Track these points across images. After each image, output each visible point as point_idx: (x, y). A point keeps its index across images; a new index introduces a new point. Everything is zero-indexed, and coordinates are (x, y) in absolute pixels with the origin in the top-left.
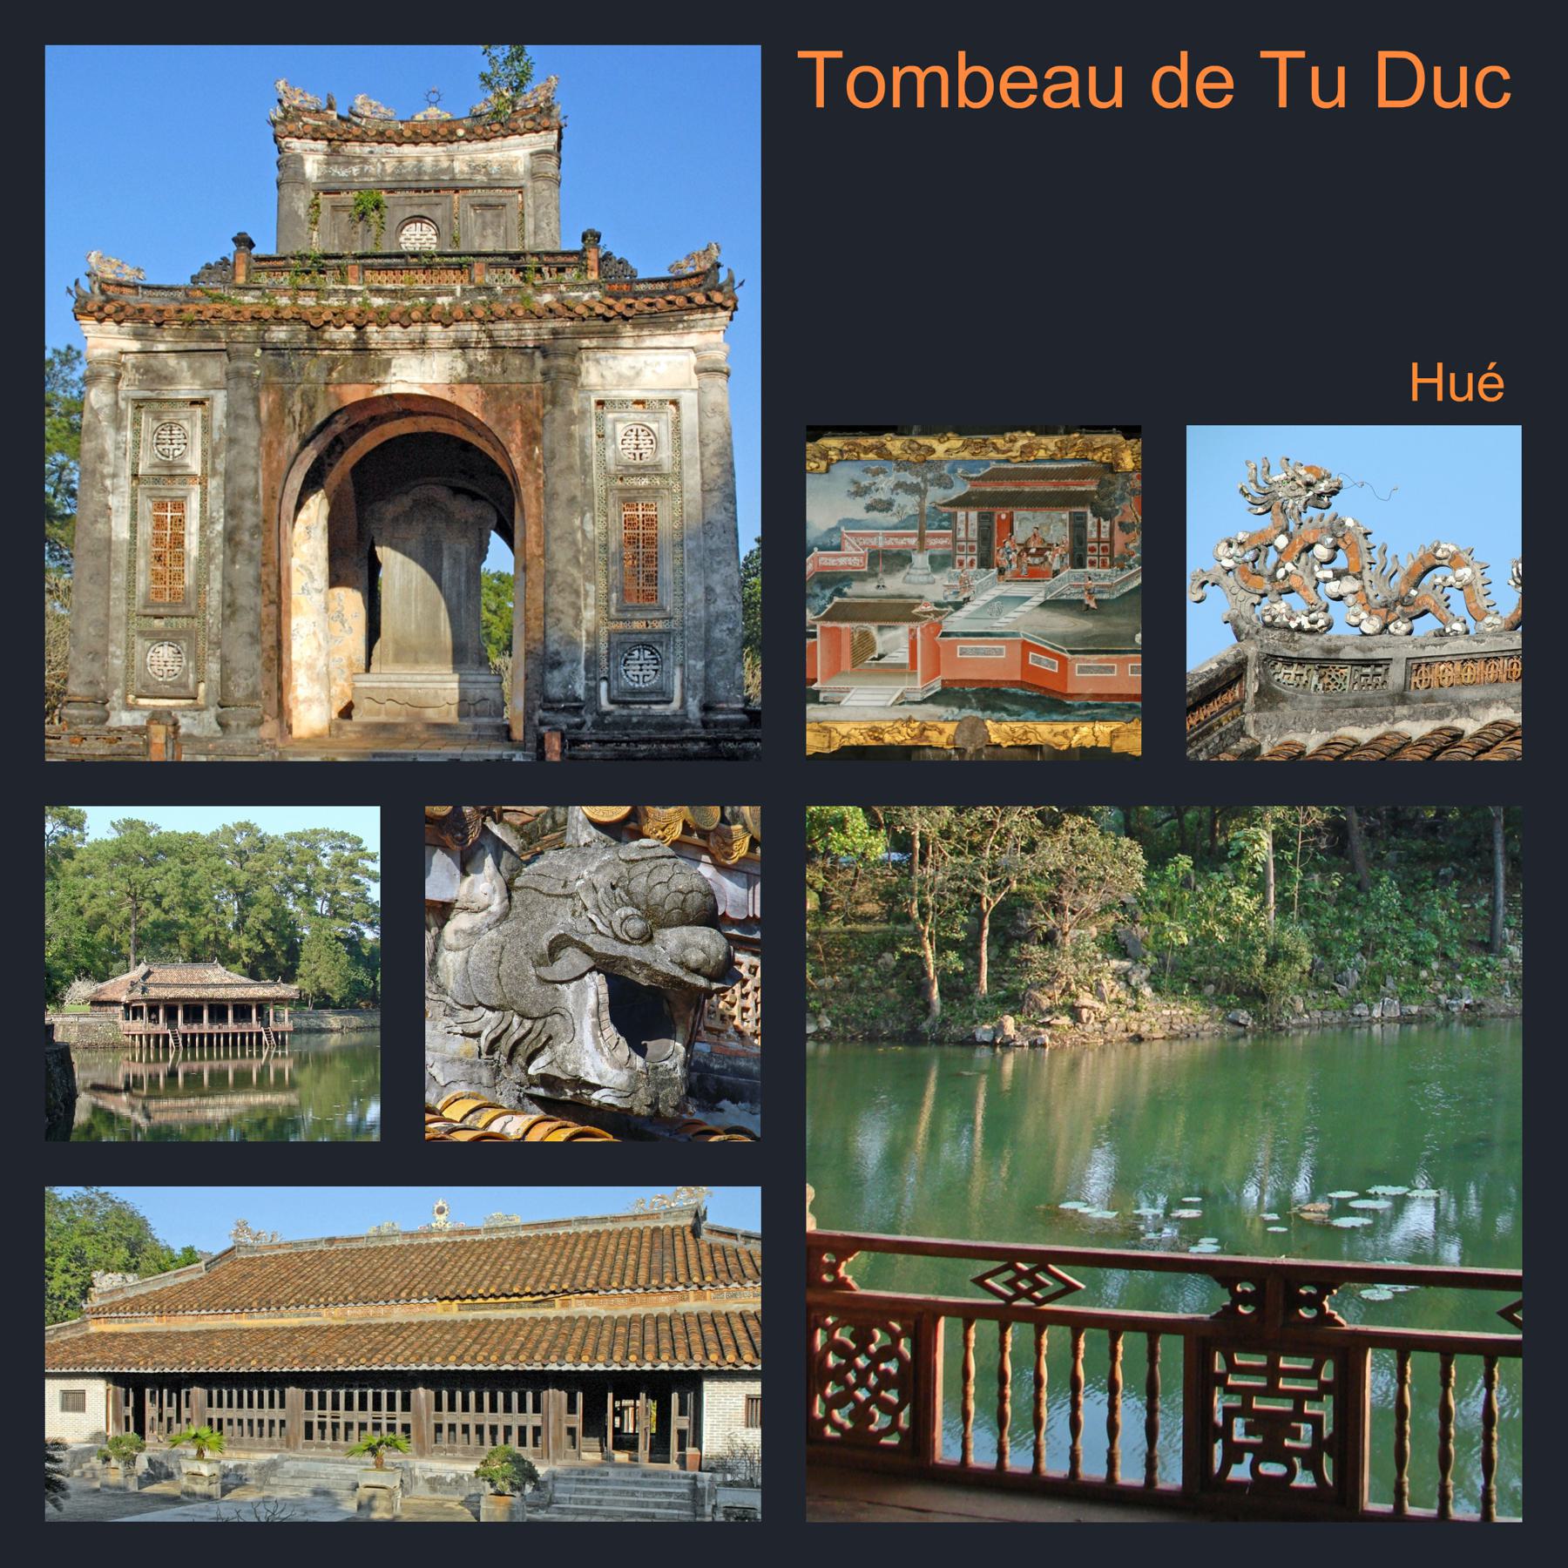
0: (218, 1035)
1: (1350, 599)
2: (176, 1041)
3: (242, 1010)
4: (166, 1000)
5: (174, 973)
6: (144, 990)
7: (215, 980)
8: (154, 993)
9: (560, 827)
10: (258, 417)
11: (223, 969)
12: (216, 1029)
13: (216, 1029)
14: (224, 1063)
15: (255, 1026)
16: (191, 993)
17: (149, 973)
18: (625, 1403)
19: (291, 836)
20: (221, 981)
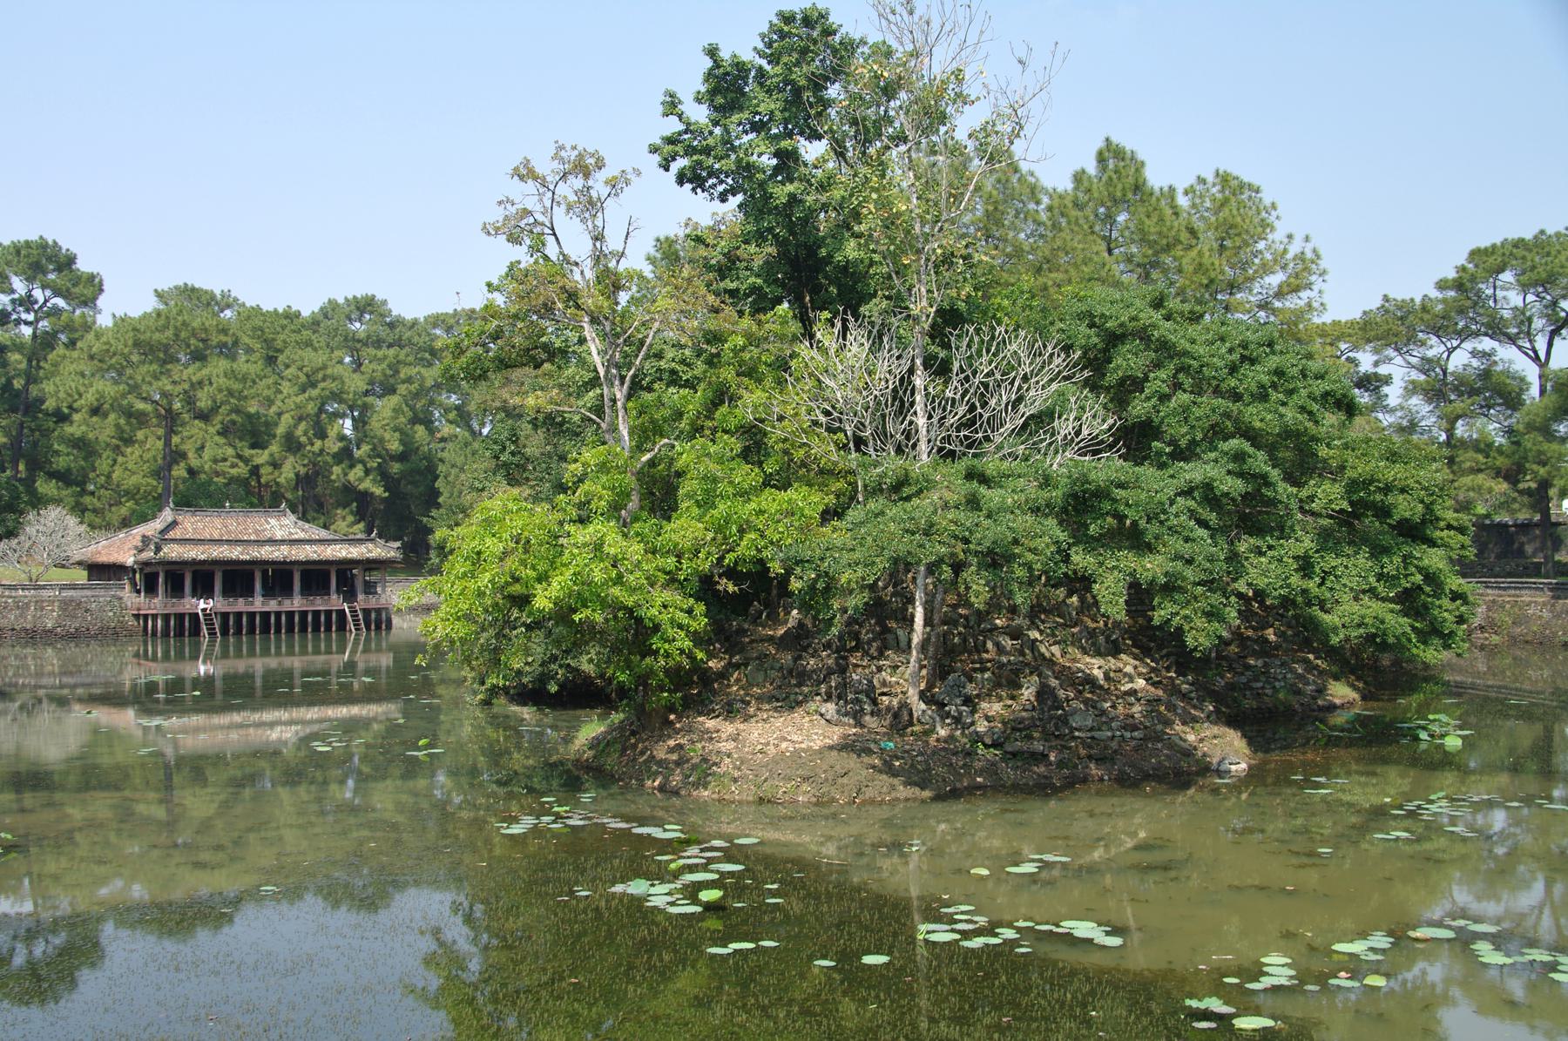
0: (278, 614)
1: (1442, 524)
2: (356, 621)
3: (316, 576)
4: (194, 562)
5: (218, 522)
6: (158, 549)
7: (279, 535)
8: (172, 552)
9: (845, 268)
10: (1322, 673)
11: (293, 518)
12: (273, 606)
13: (273, 606)
14: (252, 661)
15: (335, 602)
16: (236, 553)
17: (174, 524)
18: (1317, 570)
19: (436, 320)
20: (281, 535)
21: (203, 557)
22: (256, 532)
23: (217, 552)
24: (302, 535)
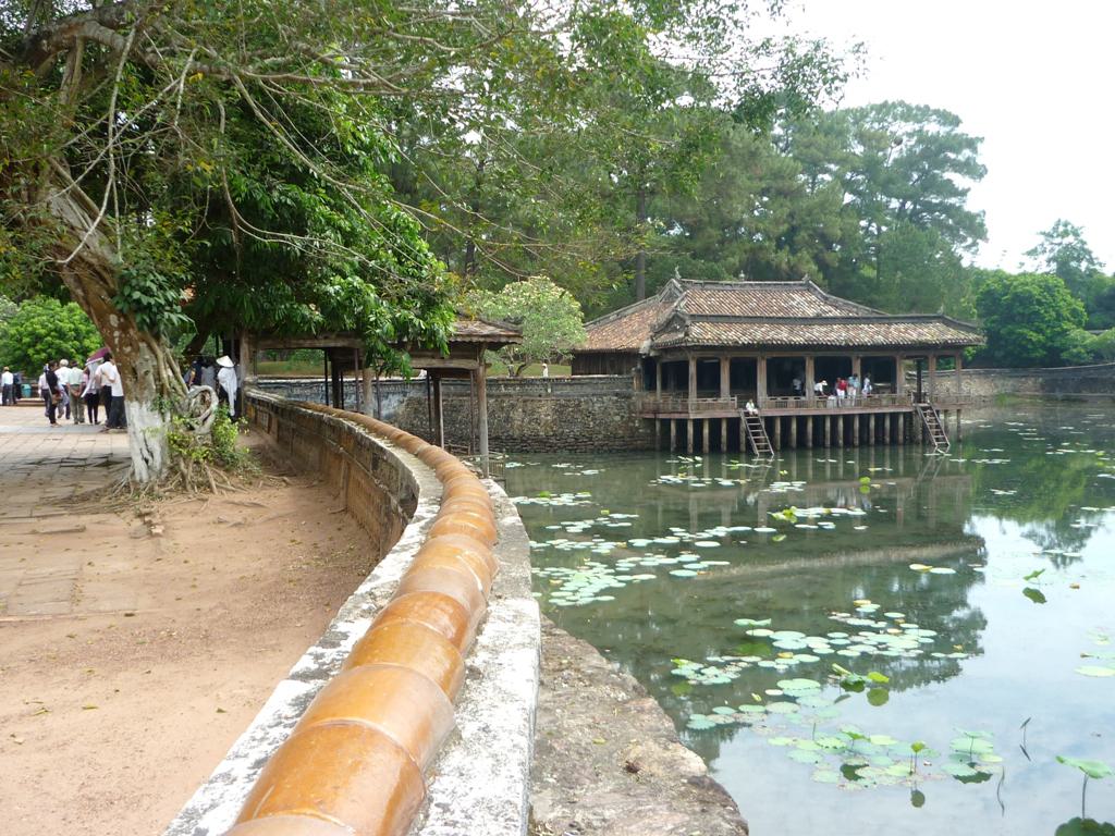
8: (703, 333)
21: (745, 340)
22: (781, 309)
23: (761, 333)
24: (837, 313)
